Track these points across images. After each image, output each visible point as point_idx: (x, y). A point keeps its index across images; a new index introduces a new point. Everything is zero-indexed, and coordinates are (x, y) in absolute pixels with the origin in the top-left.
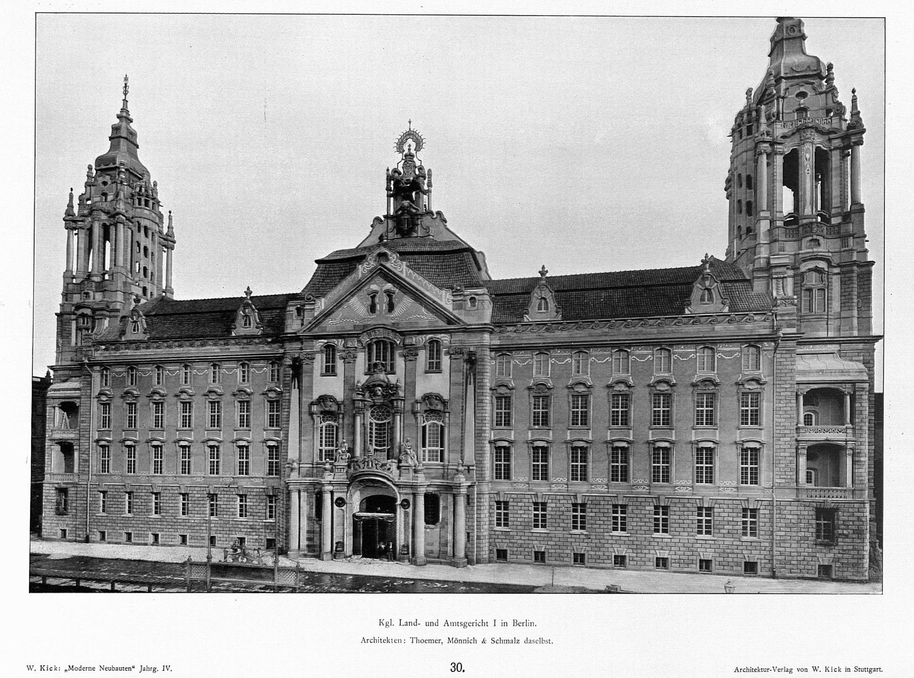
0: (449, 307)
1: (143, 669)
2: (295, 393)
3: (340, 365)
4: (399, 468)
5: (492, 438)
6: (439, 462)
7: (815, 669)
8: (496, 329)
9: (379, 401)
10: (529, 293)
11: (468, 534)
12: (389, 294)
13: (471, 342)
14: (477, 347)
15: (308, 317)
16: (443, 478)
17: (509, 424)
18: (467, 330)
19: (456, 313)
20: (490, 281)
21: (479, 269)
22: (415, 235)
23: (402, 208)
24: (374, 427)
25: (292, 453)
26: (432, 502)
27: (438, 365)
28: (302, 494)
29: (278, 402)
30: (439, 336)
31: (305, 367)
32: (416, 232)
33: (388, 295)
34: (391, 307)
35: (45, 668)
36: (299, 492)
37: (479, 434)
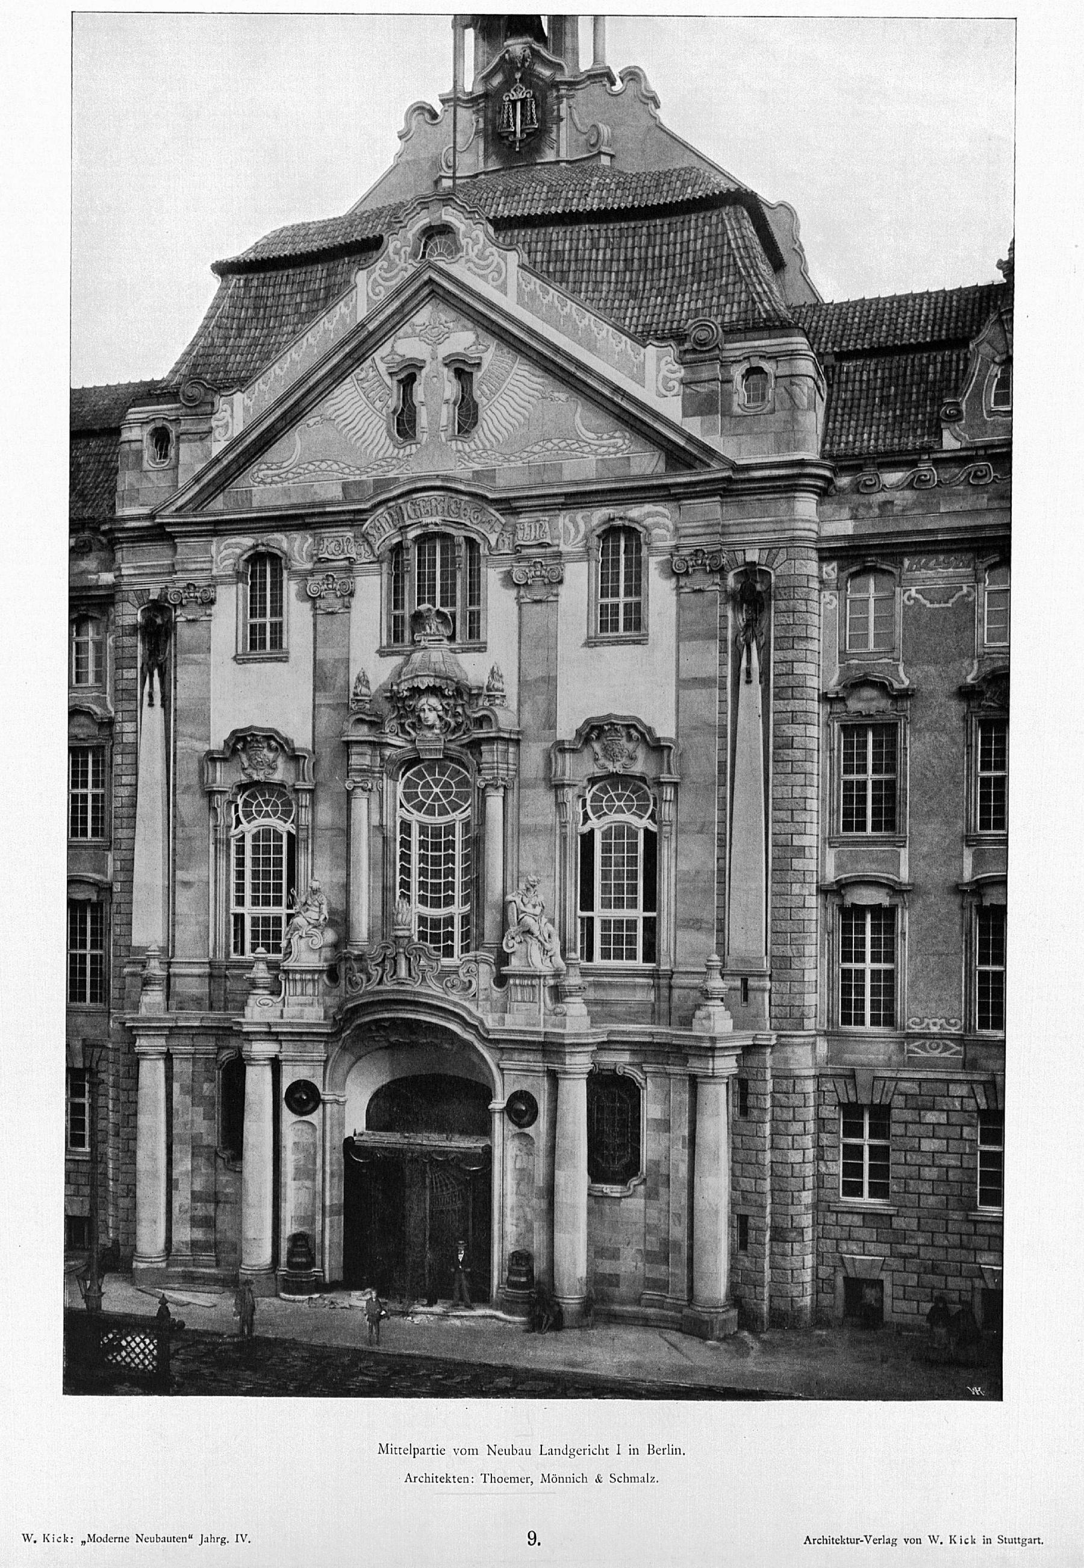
0: (671, 408)
1: (204, 1540)
2: (152, 718)
3: (297, 617)
4: (501, 980)
5: (831, 875)
6: (639, 963)
7: (933, 1539)
8: (844, 481)
9: (432, 741)
10: (964, 342)
11: (743, 1219)
12: (463, 370)
13: (752, 530)
14: (772, 548)
15: (190, 458)
16: (655, 1016)
17: (891, 825)
18: (735, 486)
19: (694, 426)
20: (818, 306)
21: (778, 265)
22: (550, 156)
23: (507, 65)
24: (415, 838)
25: (147, 930)
26: (614, 1099)
27: (635, 620)
28: (177, 1066)
29: (98, 750)
30: (635, 512)
31: (184, 632)
32: (556, 145)
33: (460, 374)
34: (467, 415)
35: (957, 1539)
36: (168, 1057)
37: (783, 860)
